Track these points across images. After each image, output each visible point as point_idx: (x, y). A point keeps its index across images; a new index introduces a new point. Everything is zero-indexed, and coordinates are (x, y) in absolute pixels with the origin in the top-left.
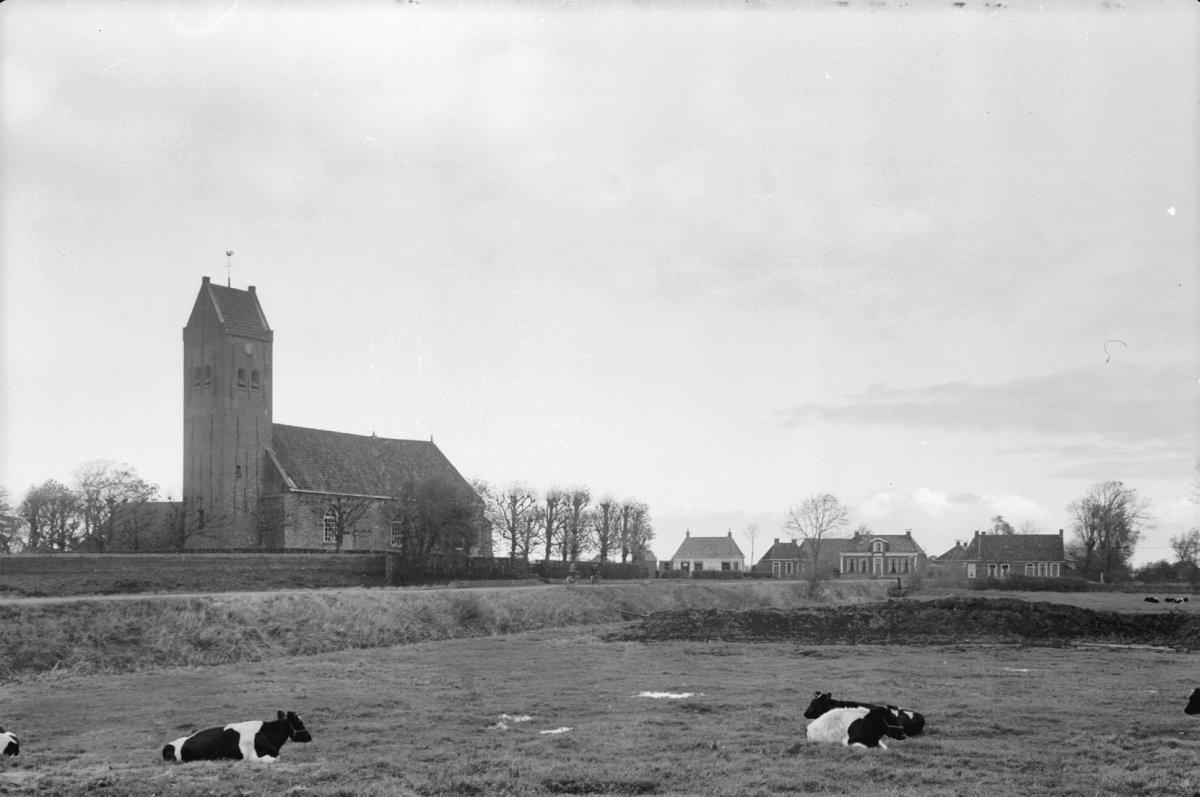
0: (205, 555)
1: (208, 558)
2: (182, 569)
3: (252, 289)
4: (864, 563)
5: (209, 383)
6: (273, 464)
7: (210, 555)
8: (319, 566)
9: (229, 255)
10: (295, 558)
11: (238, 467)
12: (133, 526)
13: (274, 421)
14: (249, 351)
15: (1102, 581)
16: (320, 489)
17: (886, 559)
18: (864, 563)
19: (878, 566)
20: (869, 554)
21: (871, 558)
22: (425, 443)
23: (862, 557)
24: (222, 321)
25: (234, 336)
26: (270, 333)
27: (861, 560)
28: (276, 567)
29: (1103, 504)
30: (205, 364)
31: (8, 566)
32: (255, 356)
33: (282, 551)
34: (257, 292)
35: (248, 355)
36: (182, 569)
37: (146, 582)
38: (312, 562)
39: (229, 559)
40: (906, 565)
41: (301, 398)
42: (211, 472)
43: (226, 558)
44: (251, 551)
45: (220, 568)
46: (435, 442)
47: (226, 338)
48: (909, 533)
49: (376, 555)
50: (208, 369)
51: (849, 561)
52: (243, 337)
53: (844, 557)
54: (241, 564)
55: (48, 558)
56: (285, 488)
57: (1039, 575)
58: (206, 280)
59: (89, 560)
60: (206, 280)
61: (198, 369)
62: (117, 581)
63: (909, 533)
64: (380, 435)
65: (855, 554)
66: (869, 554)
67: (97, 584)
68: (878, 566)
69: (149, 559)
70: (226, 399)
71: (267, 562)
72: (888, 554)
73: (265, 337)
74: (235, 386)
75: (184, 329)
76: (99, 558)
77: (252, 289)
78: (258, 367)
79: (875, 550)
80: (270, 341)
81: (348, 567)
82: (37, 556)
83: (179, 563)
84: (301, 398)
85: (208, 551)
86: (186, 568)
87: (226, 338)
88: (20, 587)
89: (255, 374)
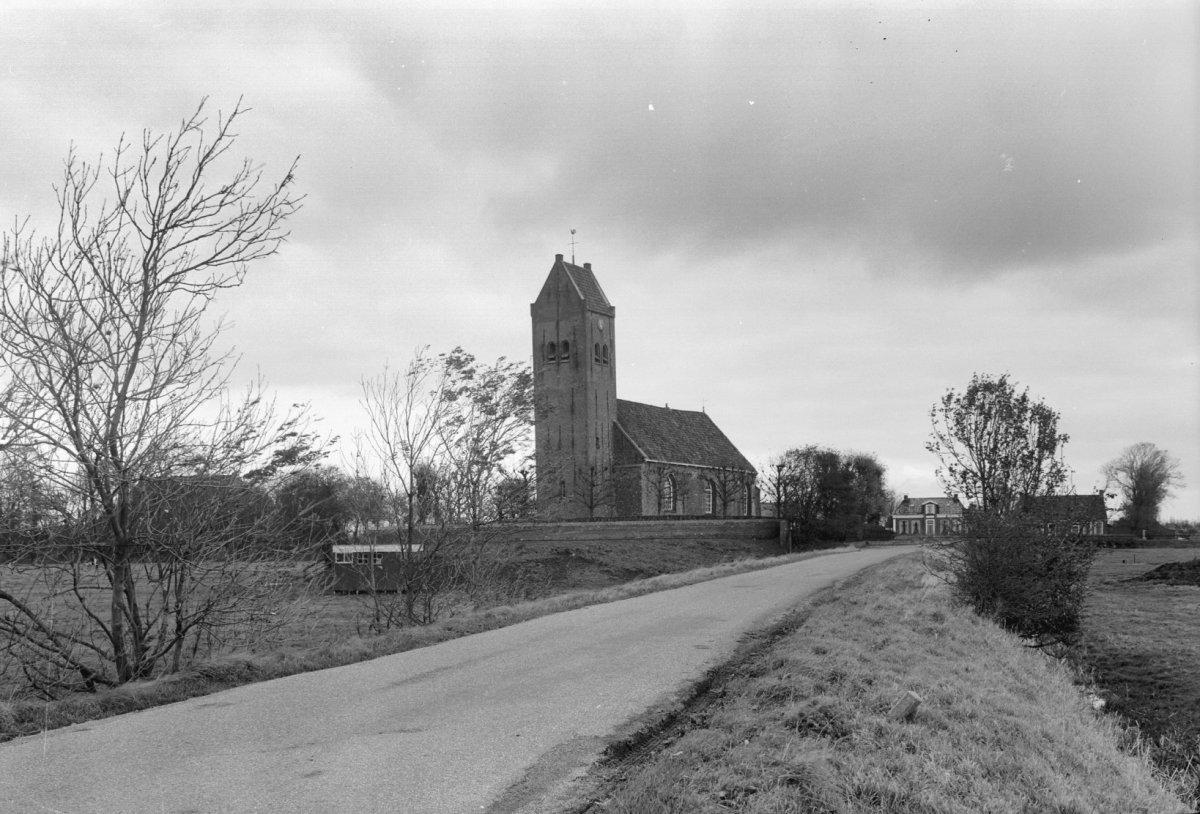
0: (617, 523)
2: (598, 537)
3: (588, 266)
4: (916, 524)
8: (715, 532)
9: (573, 233)
11: (597, 439)
13: (618, 397)
14: (601, 326)
15: (1144, 538)
17: (938, 520)
18: (916, 524)
19: (930, 527)
20: (921, 516)
21: (923, 521)
22: (694, 415)
24: (582, 298)
25: (592, 312)
26: (612, 309)
27: (913, 522)
28: (679, 533)
29: (402, 490)
30: (562, 339)
33: (640, 518)
34: (593, 269)
35: (601, 331)
38: (710, 527)
40: (904, 526)
41: (645, 374)
42: (573, 444)
44: (584, 520)
45: (630, 535)
46: (707, 412)
49: (766, 520)
50: (566, 344)
51: (901, 523)
52: (596, 313)
53: (898, 520)
57: (1095, 532)
58: (559, 257)
60: (559, 257)
61: (552, 345)
64: (672, 407)
65: (908, 517)
66: (921, 516)
68: (930, 527)
72: (939, 516)
73: (609, 313)
74: (594, 361)
77: (588, 266)
79: (927, 512)
80: (612, 317)
83: (595, 531)
84: (645, 374)
89: (605, 348)
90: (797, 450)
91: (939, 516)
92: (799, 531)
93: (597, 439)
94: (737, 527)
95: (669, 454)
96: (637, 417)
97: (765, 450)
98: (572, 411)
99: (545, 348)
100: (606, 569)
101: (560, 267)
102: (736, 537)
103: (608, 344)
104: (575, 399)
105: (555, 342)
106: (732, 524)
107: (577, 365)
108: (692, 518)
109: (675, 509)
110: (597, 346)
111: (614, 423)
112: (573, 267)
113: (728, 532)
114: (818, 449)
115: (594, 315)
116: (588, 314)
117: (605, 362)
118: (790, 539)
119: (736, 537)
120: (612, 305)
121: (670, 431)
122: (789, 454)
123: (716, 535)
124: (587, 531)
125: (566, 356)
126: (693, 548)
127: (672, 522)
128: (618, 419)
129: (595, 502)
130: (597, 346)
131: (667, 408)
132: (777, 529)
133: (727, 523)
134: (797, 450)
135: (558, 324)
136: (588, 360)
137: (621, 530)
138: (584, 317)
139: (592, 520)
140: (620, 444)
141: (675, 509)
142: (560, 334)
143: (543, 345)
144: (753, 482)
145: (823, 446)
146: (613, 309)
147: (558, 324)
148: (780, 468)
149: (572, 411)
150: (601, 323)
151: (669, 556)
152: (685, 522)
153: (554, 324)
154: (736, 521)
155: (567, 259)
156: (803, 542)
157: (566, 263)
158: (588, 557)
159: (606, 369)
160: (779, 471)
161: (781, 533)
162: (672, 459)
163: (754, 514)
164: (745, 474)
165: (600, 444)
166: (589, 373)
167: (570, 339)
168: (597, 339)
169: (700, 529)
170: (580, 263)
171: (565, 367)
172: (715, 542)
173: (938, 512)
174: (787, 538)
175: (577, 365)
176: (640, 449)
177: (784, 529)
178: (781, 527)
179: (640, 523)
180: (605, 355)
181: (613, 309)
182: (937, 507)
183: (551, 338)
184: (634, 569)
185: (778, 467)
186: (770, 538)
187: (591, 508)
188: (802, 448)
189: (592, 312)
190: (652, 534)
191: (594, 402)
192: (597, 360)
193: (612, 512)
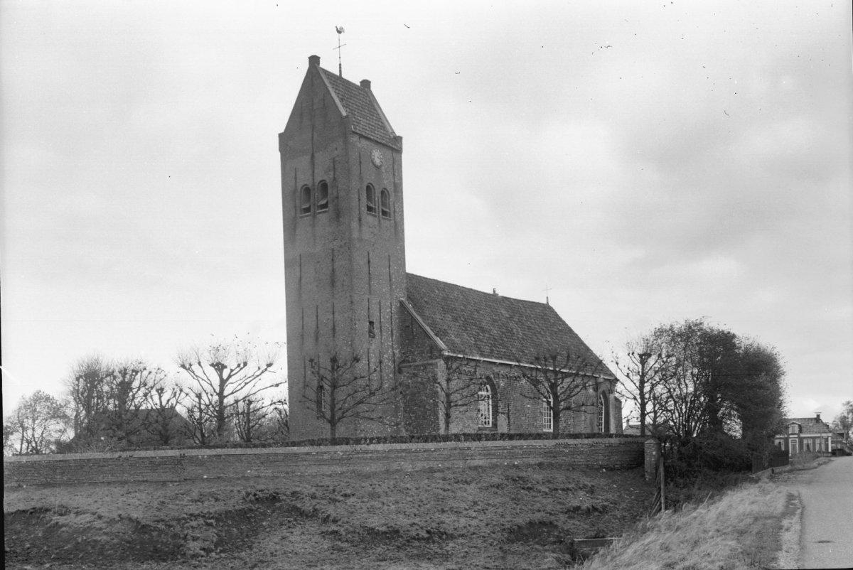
0: (372, 447)
1: (378, 452)
2: (339, 469)
3: (366, 83)
5: (325, 206)
6: (413, 319)
7: (380, 447)
9: (339, 32)
10: (505, 448)
11: (371, 323)
12: (197, 415)
14: (378, 162)
16: (472, 354)
17: (801, 440)
19: (794, 447)
23: (819, 437)
24: (344, 114)
25: (361, 136)
26: (398, 140)
30: (318, 179)
31: (62, 474)
32: (383, 168)
33: (435, 439)
35: (378, 168)
36: (339, 469)
37: (293, 494)
38: (529, 452)
39: (408, 451)
43: (404, 451)
45: (395, 466)
46: (551, 304)
47: (338, 157)
48: (818, 416)
50: (324, 186)
54: (427, 459)
55: (127, 459)
56: (434, 351)
58: (314, 60)
59: (193, 460)
60: (314, 60)
61: (307, 191)
62: (248, 494)
63: (818, 416)
67: (217, 500)
68: (794, 447)
69: (286, 455)
70: (355, 225)
71: (464, 455)
72: (802, 435)
73: (393, 145)
74: (364, 209)
75: (281, 135)
76: (210, 457)
77: (366, 83)
78: (387, 183)
80: (399, 151)
81: (580, 460)
82: (108, 455)
83: (334, 460)
85: (379, 440)
86: (345, 469)
87: (338, 157)
88: (93, 508)
90: (671, 329)
91: (802, 435)
92: (676, 456)
93: (371, 323)
94: (575, 451)
95: (487, 350)
96: (444, 299)
97: (616, 322)
98: (333, 283)
99: (298, 194)
100: (334, 527)
101: (315, 75)
102: (572, 467)
103: (390, 188)
104: (337, 264)
105: (310, 186)
106: (567, 446)
107: (338, 214)
108: (521, 436)
109: (495, 425)
110: (369, 188)
111: (401, 303)
112: (338, 81)
113: (560, 460)
114: (705, 326)
115: (364, 142)
116: (355, 139)
117: (384, 213)
118: (662, 469)
119: (572, 467)
120: (398, 134)
121: (495, 321)
122: (660, 333)
123: (540, 465)
124: (320, 462)
125: (323, 202)
126: (498, 486)
127: (467, 444)
128: (409, 298)
129: (339, 414)
130: (369, 188)
131: (495, 295)
132: (641, 454)
133: (558, 445)
134: (671, 329)
135: (313, 156)
136: (355, 203)
137: (378, 459)
138: (346, 142)
139: (335, 442)
140: (410, 333)
141: (495, 425)
142: (316, 171)
143: (295, 192)
144: (611, 391)
145: (717, 322)
146: (400, 138)
147: (313, 156)
148: (644, 358)
149: (333, 283)
150: (377, 156)
151: (451, 503)
152: (490, 444)
153: (308, 158)
154: (571, 442)
155: (328, 64)
156: (682, 475)
157: (325, 72)
158: (308, 506)
159: (385, 223)
160: (643, 363)
161: (647, 459)
162: (490, 355)
163: (613, 430)
164: (586, 365)
165: (376, 331)
166: (355, 225)
167: (328, 179)
168: (370, 178)
169: (514, 456)
170: (354, 77)
171: (323, 218)
172: (538, 476)
173: (801, 431)
174: (657, 469)
175: (338, 214)
176: (438, 340)
177: (651, 453)
178: (647, 451)
179: (431, 446)
180: (384, 203)
181: (400, 138)
182: (800, 427)
183: (304, 179)
184: (384, 529)
185: (641, 356)
186: (630, 468)
187: (333, 422)
188: (679, 323)
189: (361, 136)
190: (431, 464)
191: (366, 269)
192: (370, 209)
193: (398, 431)
